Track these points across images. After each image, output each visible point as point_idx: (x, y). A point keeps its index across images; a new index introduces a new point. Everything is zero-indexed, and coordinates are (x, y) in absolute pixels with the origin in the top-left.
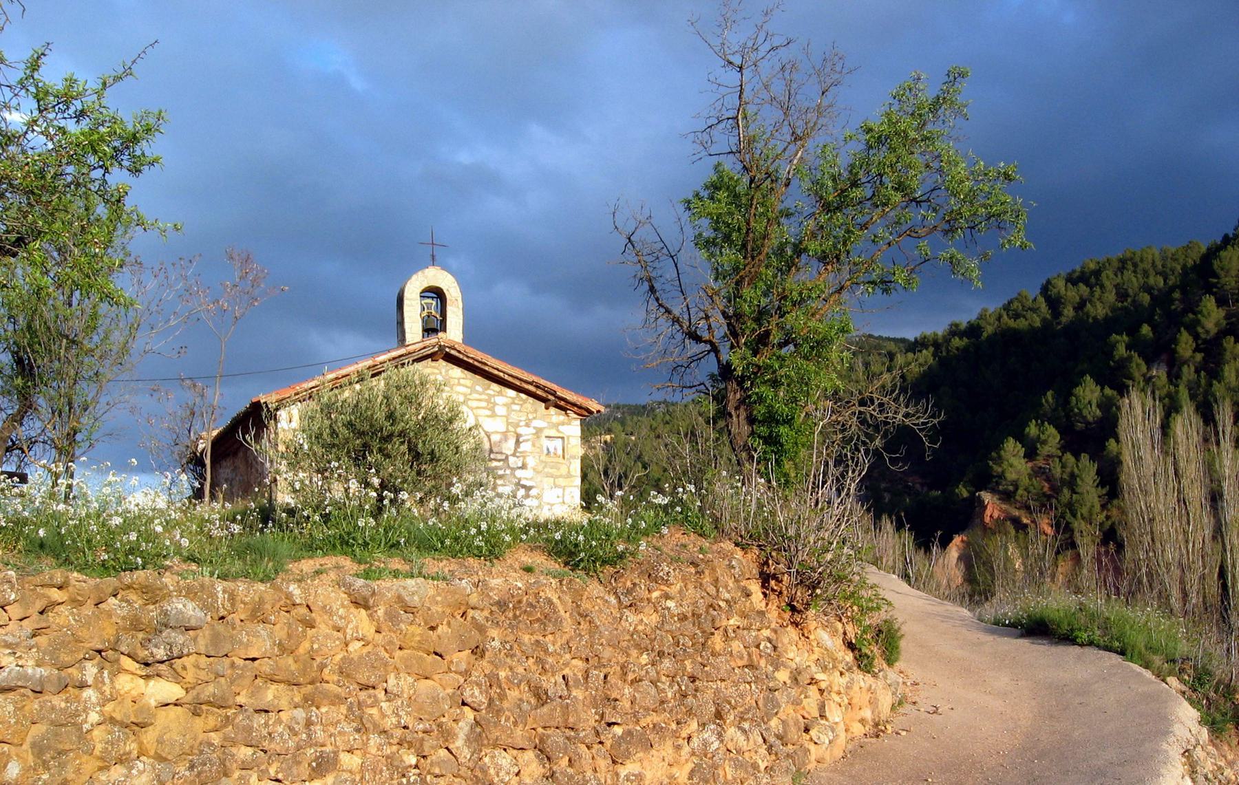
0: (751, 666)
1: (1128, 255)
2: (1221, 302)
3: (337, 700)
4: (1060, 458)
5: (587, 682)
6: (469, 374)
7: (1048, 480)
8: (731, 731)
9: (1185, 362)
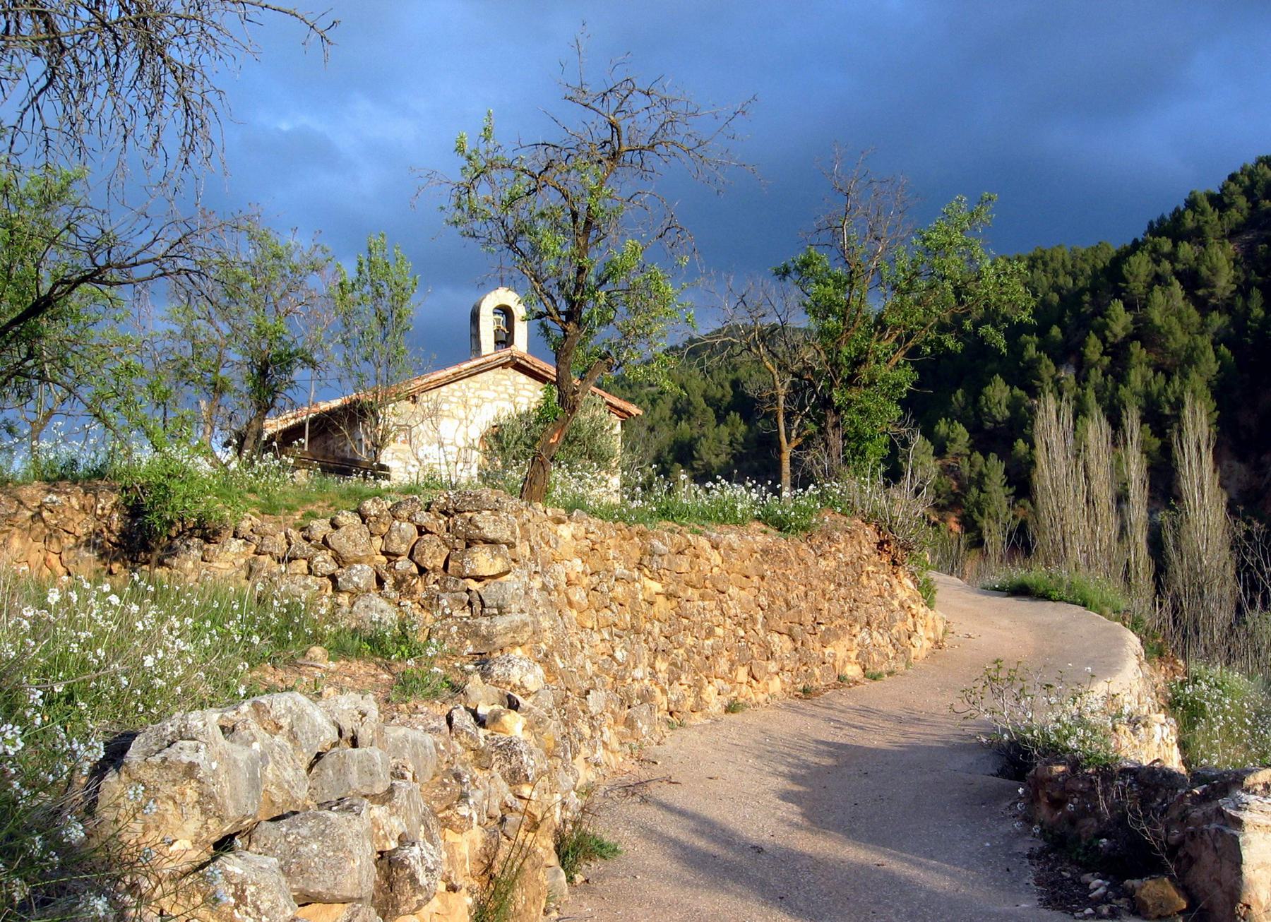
0: (881, 596)
1: (1039, 254)
2: (1129, 307)
3: (712, 599)
4: (969, 457)
7: (956, 478)
8: (875, 634)
9: (1093, 365)
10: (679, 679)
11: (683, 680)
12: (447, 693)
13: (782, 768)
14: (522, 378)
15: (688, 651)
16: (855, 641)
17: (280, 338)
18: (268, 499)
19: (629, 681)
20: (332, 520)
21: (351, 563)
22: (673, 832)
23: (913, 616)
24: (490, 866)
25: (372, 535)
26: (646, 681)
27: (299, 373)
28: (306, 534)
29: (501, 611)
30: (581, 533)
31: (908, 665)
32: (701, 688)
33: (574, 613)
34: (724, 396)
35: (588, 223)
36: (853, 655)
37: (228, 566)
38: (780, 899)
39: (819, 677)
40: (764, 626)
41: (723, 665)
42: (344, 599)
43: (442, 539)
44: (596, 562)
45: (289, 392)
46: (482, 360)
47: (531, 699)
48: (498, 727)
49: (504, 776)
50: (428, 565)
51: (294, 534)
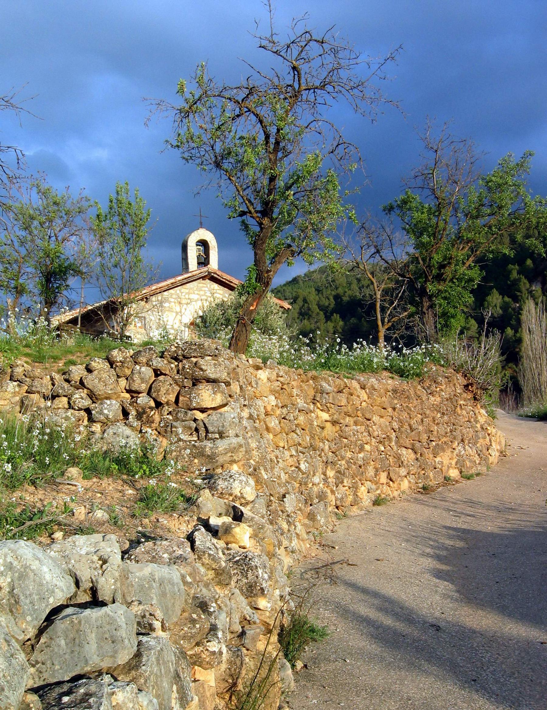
5: (423, 423)
6: (222, 288)
8: (467, 447)
10: (342, 482)
11: (345, 484)
12: (182, 505)
13: (428, 550)
14: (216, 286)
15: (348, 462)
16: (455, 453)
17: (59, 257)
18: (38, 352)
19: (310, 485)
20: (87, 365)
21: (102, 399)
22: (364, 610)
23: (489, 435)
24: (235, 684)
25: (118, 377)
26: (321, 485)
27: (72, 281)
28: (66, 377)
29: (222, 435)
30: (274, 377)
31: (488, 468)
32: (357, 488)
33: (271, 436)
34: (329, 304)
35: (277, 143)
36: (454, 462)
37: (6, 402)
38: (474, 681)
39: (433, 479)
40: (397, 443)
41: (371, 472)
42: (96, 428)
43: (174, 379)
44: (284, 398)
45: (65, 292)
46: (190, 275)
47: (249, 507)
48: (230, 538)
49: (241, 590)
50: (163, 400)
51: (57, 377)
